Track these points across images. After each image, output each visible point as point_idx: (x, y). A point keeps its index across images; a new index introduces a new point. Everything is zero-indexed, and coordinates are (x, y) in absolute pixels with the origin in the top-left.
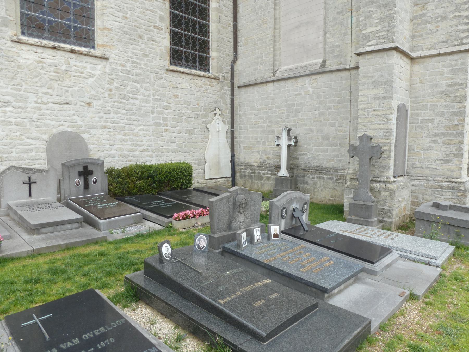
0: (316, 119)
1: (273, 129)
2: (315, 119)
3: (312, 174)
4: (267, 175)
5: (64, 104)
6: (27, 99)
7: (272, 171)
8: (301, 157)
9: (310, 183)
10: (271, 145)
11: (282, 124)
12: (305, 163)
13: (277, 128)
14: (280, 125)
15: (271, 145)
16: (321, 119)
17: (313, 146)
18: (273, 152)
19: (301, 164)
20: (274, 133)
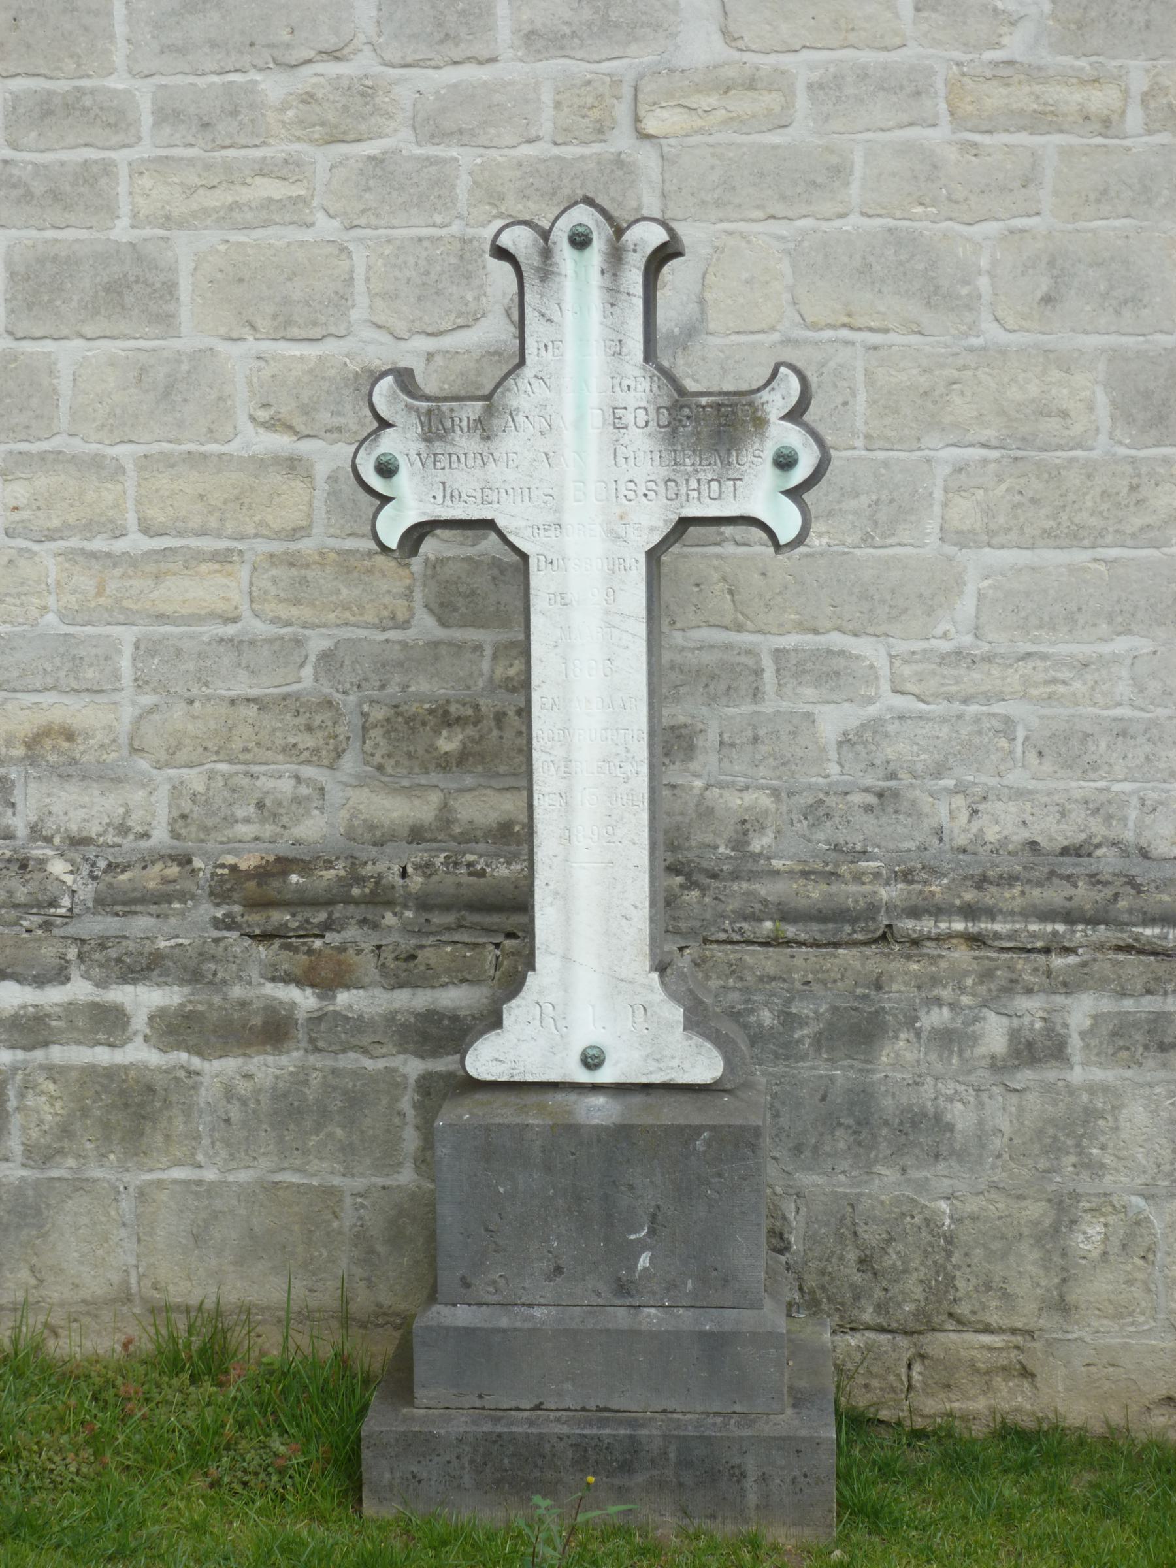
0: (1022, 97)
1: (122, 231)
2: (996, 97)
3: (1012, 986)
4: (103, 1056)
5: (906, 545)
6: (25, 1161)
7: (193, 977)
8: (740, 710)
9: (982, 1136)
10: (89, 528)
11: (321, 158)
12: (817, 812)
13: (229, 216)
14: (289, 168)
15: (89, 528)
16: (1099, 99)
17: (963, 539)
18: (145, 649)
19: (745, 827)
20: (166, 321)
